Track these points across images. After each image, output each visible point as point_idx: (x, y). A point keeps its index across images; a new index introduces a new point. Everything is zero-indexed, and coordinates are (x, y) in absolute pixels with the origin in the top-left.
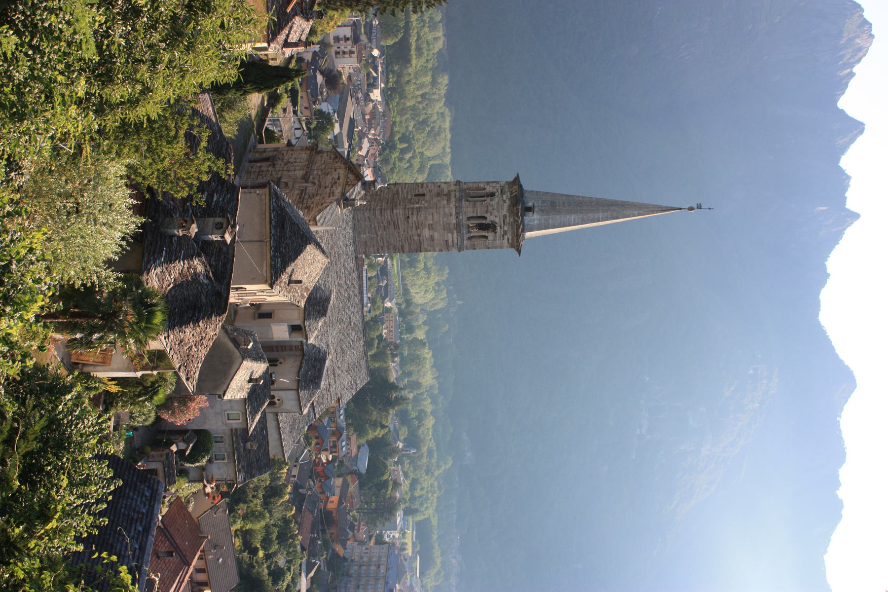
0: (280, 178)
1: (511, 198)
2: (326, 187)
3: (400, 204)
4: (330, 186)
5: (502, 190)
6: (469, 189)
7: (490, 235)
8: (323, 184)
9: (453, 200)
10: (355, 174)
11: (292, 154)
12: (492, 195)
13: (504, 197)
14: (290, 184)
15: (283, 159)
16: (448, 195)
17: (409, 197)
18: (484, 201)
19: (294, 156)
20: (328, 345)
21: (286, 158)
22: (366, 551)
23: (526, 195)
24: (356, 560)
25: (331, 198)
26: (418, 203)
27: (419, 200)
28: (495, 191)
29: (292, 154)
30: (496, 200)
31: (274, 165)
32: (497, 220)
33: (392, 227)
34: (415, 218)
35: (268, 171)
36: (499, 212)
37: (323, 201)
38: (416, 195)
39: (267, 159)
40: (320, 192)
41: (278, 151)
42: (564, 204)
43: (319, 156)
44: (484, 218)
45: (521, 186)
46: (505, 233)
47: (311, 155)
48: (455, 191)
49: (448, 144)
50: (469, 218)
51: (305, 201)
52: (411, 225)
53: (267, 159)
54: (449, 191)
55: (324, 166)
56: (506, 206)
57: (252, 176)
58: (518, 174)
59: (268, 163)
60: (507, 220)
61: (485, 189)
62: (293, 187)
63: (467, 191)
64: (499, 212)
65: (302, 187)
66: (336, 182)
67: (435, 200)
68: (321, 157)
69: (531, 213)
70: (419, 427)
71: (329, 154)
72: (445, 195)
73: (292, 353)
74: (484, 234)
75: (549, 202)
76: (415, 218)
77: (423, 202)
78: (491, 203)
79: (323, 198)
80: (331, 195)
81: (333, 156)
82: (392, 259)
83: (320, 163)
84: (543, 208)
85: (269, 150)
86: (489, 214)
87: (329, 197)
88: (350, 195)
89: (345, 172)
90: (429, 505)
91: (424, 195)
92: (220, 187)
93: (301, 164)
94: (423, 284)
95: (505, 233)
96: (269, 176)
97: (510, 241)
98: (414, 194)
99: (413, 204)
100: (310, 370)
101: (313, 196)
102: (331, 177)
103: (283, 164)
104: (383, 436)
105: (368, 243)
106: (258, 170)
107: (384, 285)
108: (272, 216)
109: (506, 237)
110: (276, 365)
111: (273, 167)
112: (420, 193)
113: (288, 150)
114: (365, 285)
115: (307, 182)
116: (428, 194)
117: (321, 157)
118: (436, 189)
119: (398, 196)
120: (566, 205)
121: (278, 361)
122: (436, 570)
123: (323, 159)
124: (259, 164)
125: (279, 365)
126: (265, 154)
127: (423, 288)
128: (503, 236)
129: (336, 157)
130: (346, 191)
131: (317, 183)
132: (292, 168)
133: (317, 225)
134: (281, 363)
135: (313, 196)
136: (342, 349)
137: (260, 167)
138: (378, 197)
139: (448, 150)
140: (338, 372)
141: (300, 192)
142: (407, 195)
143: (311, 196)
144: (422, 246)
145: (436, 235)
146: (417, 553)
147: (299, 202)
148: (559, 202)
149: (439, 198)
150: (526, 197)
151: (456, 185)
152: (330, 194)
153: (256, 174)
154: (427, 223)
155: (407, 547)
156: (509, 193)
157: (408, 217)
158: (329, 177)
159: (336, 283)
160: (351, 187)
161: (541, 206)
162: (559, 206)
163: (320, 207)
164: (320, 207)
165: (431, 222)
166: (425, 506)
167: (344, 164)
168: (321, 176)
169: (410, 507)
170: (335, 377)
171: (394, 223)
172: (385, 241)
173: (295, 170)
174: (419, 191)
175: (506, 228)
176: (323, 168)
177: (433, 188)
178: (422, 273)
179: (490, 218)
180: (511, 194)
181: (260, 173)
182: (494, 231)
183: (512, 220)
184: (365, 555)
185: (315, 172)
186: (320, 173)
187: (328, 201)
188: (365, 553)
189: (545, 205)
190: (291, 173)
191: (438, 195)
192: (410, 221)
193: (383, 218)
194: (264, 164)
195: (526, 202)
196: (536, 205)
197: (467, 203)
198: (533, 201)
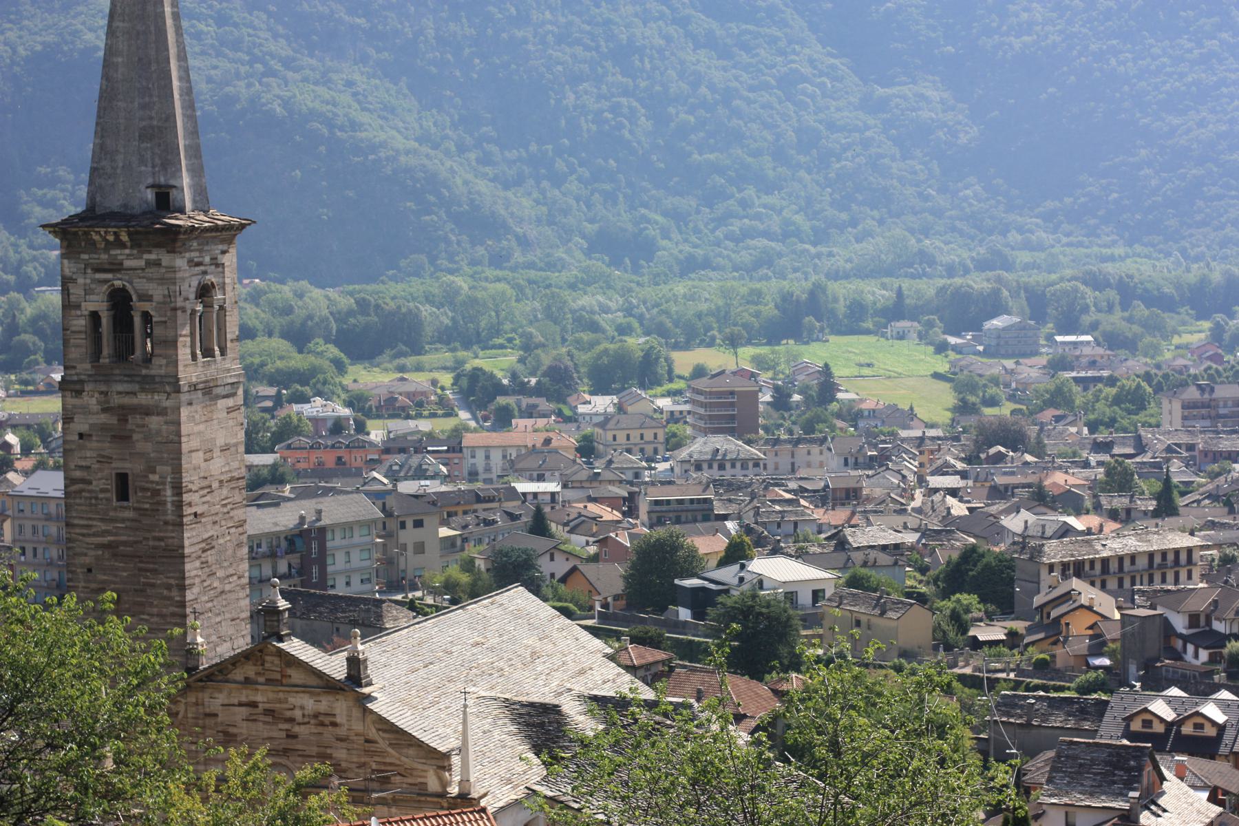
2: (291, 736)
3: (160, 539)
4: (286, 726)
6: (96, 354)
9: (143, 399)
12: (120, 301)
17: (129, 514)
18: (147, 317)
22: (29, 552)
24: (56, 575)
25: (338, 720)
26: (156, 493)
27: (144, 489)
40: (314, 750)
54: (105, 410)
56: (166, 259)
58: (44, 226)
61: (95, 317)
63: (104, 361)
66: (269, 712)
67: (141, 446)
69: (174, 193)
75: (144, 145)
80: (327, 720)
84: (158, 161)
87: (334, 724)
89: (220, 691)
98: (115, 503)
102: (245, 724)
118: (94, 445)
119: (125, 543)
120: (147, 99)
128: (217, 265)
129: (970, 708)
142: (123, 520)
148: (141, 119)
149: (135, 437)
150: (125, 206)
151: (79, 393)
152: (322, 724)
156: (113, 252)
157: (195, 515)
161: (153, 167)
162: (151, 118)
163: (382, 744)
164: (382, 744)
165: (201, 454)
171: (204, 551)
175: (207, 259)
180: (122, 245)
184: (39, 555)
188: (35, 555)
189: (148, 155)
191: (122, 437)
192: (199, 510)
196: (150, 181)
198: (142, 187)
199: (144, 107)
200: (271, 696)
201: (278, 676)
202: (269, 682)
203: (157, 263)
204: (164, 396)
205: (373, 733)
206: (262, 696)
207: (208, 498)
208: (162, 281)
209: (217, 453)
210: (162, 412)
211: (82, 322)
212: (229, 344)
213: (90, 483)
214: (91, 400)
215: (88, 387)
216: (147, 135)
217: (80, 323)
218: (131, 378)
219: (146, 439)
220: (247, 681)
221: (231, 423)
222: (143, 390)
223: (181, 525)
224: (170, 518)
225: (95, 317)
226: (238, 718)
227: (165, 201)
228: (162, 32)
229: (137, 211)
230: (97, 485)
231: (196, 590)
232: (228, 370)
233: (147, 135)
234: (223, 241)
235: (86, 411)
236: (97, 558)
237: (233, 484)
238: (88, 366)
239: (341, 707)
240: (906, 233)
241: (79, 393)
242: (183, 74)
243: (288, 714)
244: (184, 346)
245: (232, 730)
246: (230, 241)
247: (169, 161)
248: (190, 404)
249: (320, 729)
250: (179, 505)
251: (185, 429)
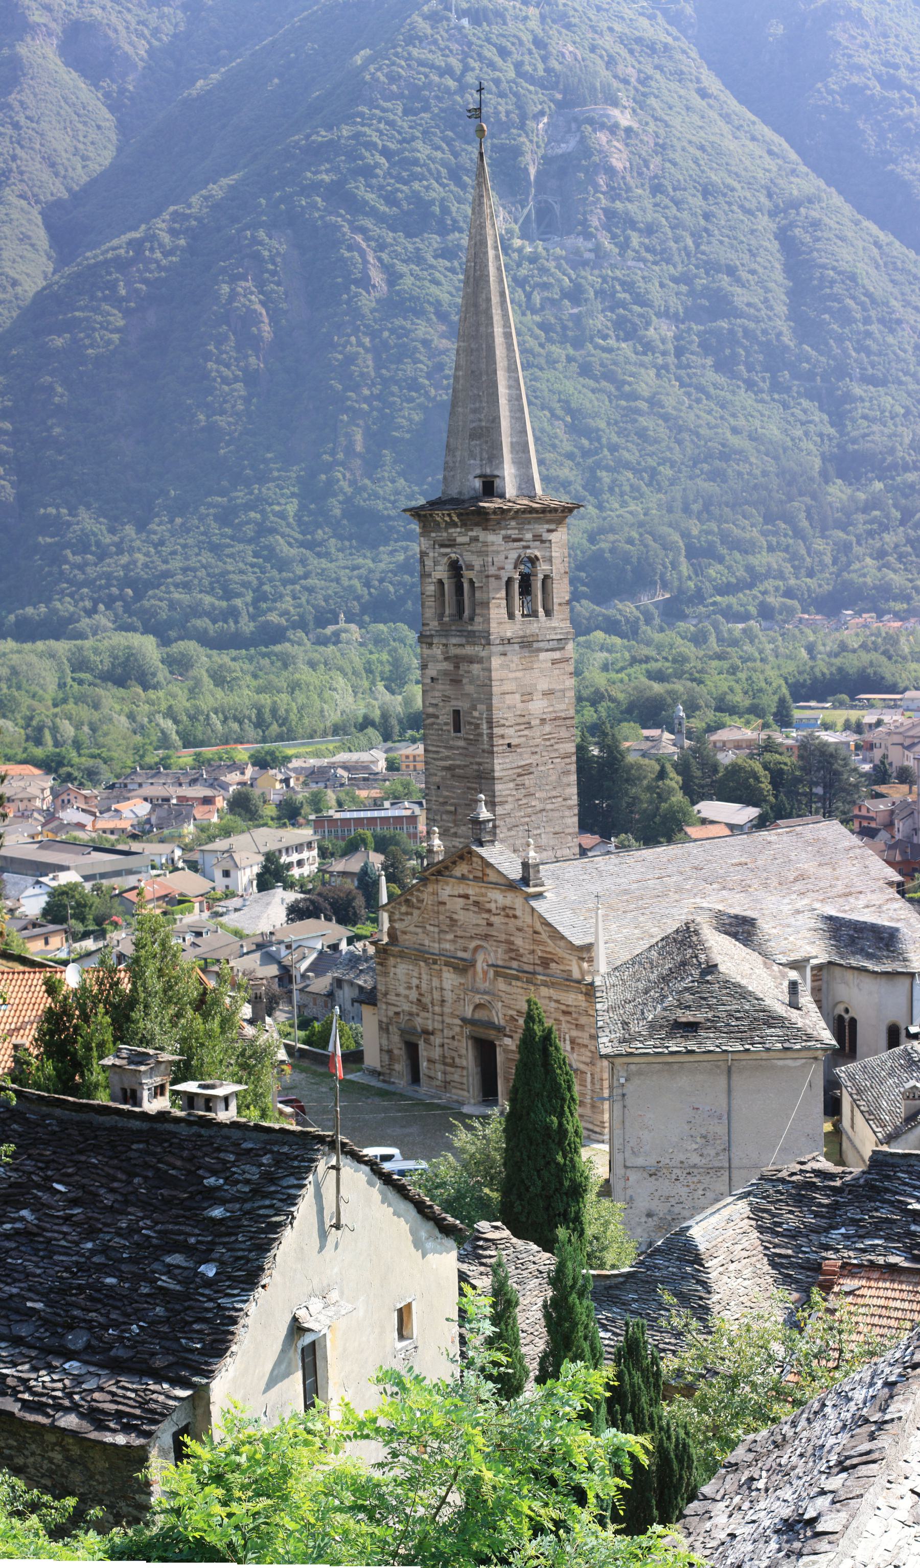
0: (464, 1020)
1: (464, 525)
2: (490, 925)
3: (480, 764)
4: (486, 916)
6: (441, 616)
7: (543, 568)
9: (469, 650)
10: (454, 863)
11: (398, 995)
12: (455, 568)
13: (460, 540)
14: (478, 999)
17: (461, 743)
18: (471, 582)
19: (402, 991)
20: (798, 912)
21: (406, 1007)
23: (453, 492)
25: (518, 913)
26: (477, 726)
27: (470, 723)
28: (445, 560)
29: (398, 995)
30: (466, 556)
31: (426, 1032)
33: (527, 780)
34: (511, 731)
35: (442, 1046)
36: (498, 552)
37: (530, 931)
38: (457, 729)
39: (412, 1050)
40: (503, 937)
42: (474, 411)
43: (402, 938)
44: (509, 581)
45: (434, 504)
46: (538, 538)
47: (402, 955)
48: (445, 645)
49: (28, 646)
50: (511, 616)
51: (529, 968)
53: (412, 1050)
54: (447, 659)
55: (432, 929)
56: (483, 535)
60: (514, 533)
61: (440, 582)
62: (485, 993)
63: (446, 619)
64: (498, 552)
65: (485, 973)
66: (476, 903)
67: (469, 689)
68: (404, 933)
69: (497, 482)
70: (612, 699)
71: (396, 917)
72: (457, 667)
73: (824, 987)
78: (477, 568)
79: (519, 930)
80: (511, 913)
81: (404, 909)
82: (288, 759)
83: (421, 936)
84: (485, 455)
85: (385, 1042)
86: (502, 573)
87: (515, 917)
88: (515, 873)
91: (457, 713)
93: (424, 976)
94: (320, 695)
95: (538, 538)
97: (553, 527)
99: (481, 735)
101: (513, 952)
104: (678, 774)
105: (557, 829)
106: (439, 1066)
107: (345, 774)
108: (675, 1049)
109: (546, 536)
110: (853, 1021)
111: (432, 1033)
112: (451, 721)
113: (387, 1004)
114: (355, 815)
115: (472, 964)
116: (454, 703)
117: (404, 933)
118: (440, 687)
119: (459, 767)
121: (840, 1017)
122: (884, 659)
123: (412, 929)
124: (424, 1064)
126: (396, 1052)
128: (543, 542)
131: (479, 942)
132: (436, 995)
133: (591, 945)
134: (847, 1011)
135: (512, 950)
136: (796, 880)
137: (430, 1061)
141: (500, 979)
142: (458, 748)
143: (513, 955)
144: (563, 715)
145: (543, 685)
147: (529, 982)
149: (465, 681)
150: (460, 493)
152: (507, 916)
153: (449, 1069)
154: (520, 705)
155: (853, 720)
157: (509, 745)
158: (461, 916)
159: (677, 897)
160: (488, 871)
163: (544, 936)
164: (544, 936)
166: (763, 685)
167: (425, 885)
168: (459, 933)
169: (775, 715)
170: (850, 894)
171: (519, 775)
172: (554, 793)
173: (442, 989)
174: (446, 724)
175: (529, 536)
177: (437, 694)
178: (301, 698)
180: (455, 525)
181: (448, 1063)
182: (533, 561)
185: (447, 946)
186: (450, 937)
190: (449, 996)
191: (456, 681)
192: (514, 742)
194: (423, 1052)
195: (472, 493)
196: (478, 472)
197: (478, 619)
198: (471, 477)
201: (480, 874)
202: (476, 878)
207: (526, 732)
208: (480, 553)
209: (537, 696)
210: (480, 661)
214: (437, 651)
215: (435, 641)
217: (431, 589)
218: (461, 633)
219: (471, 682)
220: (463, 878)
221: (556, 672)
223: (492, 753)
224: (486, 747)
225: (440, 582)
227: (490, 488)
228: (491, 349)
229: (466, 497)
231: (508, 807)
234: (549, 522)
236: (443, 778)
237: (558, 723)
239: (516, 901)
241: (430, 645)
243: (488, 906)
244: (499, 606)
245: (455, 917)
247: (495, 455)
249: (507, 920)
250: (491, 736)
251: (494, 675)
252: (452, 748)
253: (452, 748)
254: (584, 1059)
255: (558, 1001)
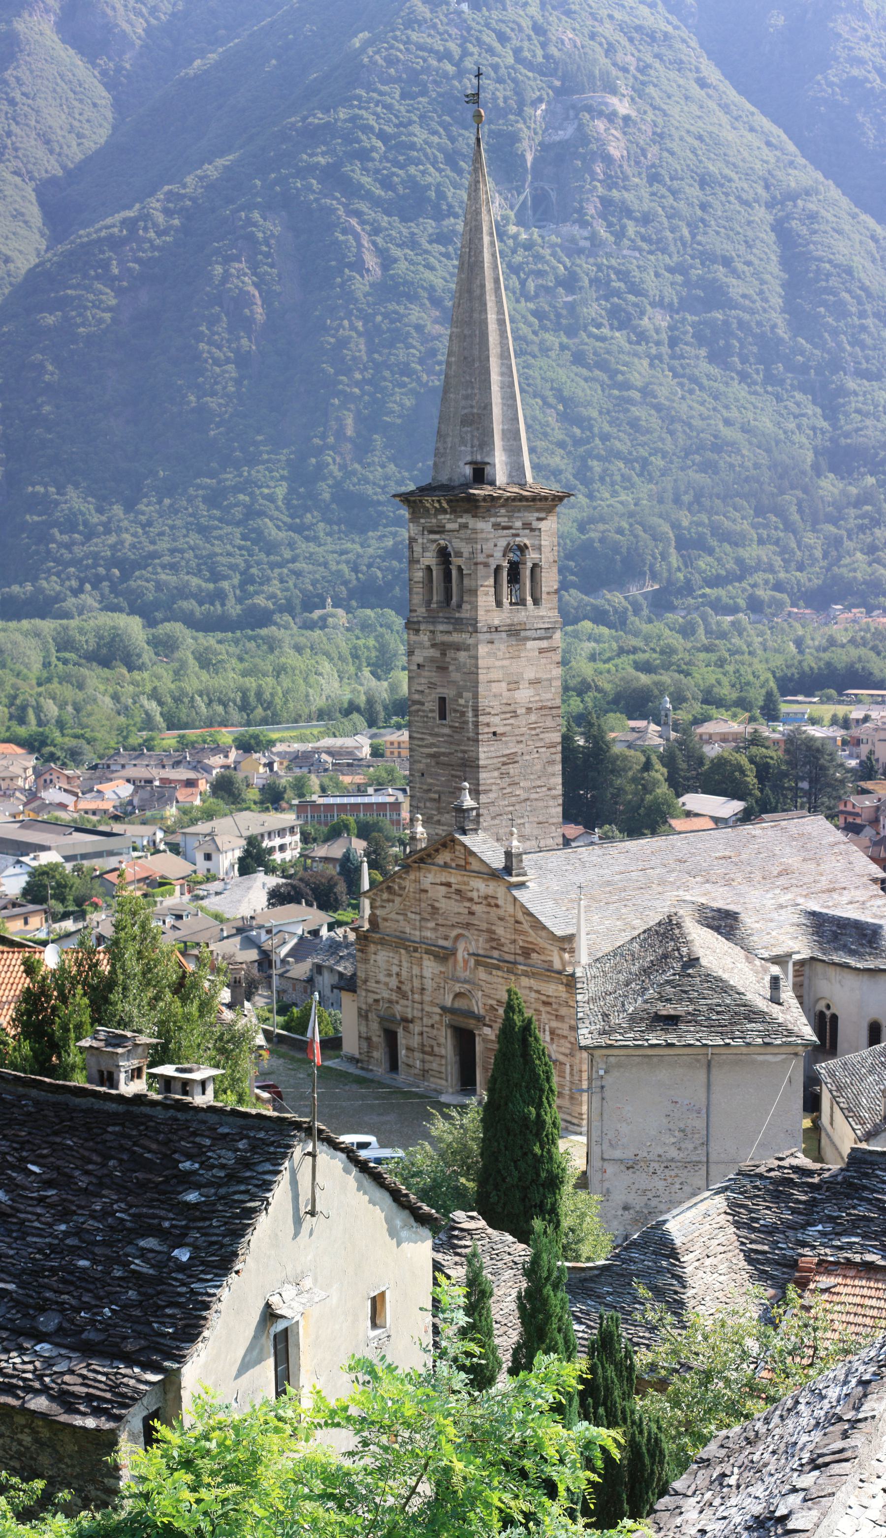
0: (443, 1008)
1: (454, 511)
2: (471, 913)
3: (465, 752)
4: (468, 904)
5: (431, 532)
6: (429, 602)
8: (465, 919)
9: (456, 637)
10: (437, 851)
11: (377, 982)
12: (444, 555)
14: (458, 988)
15: (390, 1002)
16: (444, 648)
17: (446, 731)
18: (460, 569)
19: (382, 978)
20: (781, 907)
23: (444, 478)
25: (500, 902)
26: (463, 714)
27: (456, 711)
28: (434, 546)
31: (406, 1020)
32: (502, 543)
33: (512, 769)
34: (496, 720)
35: (421, 1034)
36: (487, 540)
38: (443, 716)
39: (391, 1038)
40: (484, 926)
41: (367, 1011)
43: (382, 925)
45: (424, 490)
46: (527, 526)
47: (382, 942)
48: (432, 632)
49: (13, 624)
50: (499, 604)
52: (509, 728)
53: (391, 1038)
54: (433, 646)
56: (472, 522)
57: (435, 1066)
58: (394, 496)
59: (401, 1033)
60: (503, 521)
61: (429, 569)
62: (466, 981)
63: (434, 606)
64: (487, 540)
65: (466, 962)
66: (458, 892)
67: (455, 676)
68: (385, 920)
69: (488, 469)
70: (599, 690)
71: (378, 904)
72: (444, 654)
74: (528, 572)
76: (496, 720)
77: (462, 701)
78: (466, 555)
80: (493, 902)
81: (385, 896)
83: (402, 923)
84: (476, 442)
85: (364, 1029)
86: (491, 560)
87: (497, 906)
89: (430, 871)
90: (749, 670)
91: (442, 700)
92: (865, 1194)
94: (305, 680)
95: (527, 526)
96: (435, 1032)
97: (542, 515)
99: (466, 722)
100: (845, 946)
102: (444, 900)
103: (403, 1002)
104: (664, 765)
106: (417, 1055)
107: (329, 759)
109: (535, 524)
110: (834, 1018)
111: (412, 1021)
112: (436, 708)
114: (339, 800)
115: (453, 952)
116: (440, 690)
117: (385, 920)
118: (426, 674)
119: (444, 754)
123: (393, 916)
125: (833, 1010)
126: (375, 1039)
127: (313, 678)
128: (532, 530)
130: (484, 869)
131: (460, 931)
132: (416, 983)
134: (828, 1007)
135: (493, 940)
136: (780, 875)
137: (409, 1049)
138: (443, 798)
139: (25, 624)
140: (824, 883)
141: (481, 968)
142: (443, 735)
143: (494, 944)
145: (530, 674)
146: (840, 694)
148: (464, 408)
149: (451, 668)
150: (450, 479)
151: (417, 631)
152: (489, 905)
153: (427, 1057)
154: (506, 694)
155: (841, 715)
156: (440, 517)
157: (494, 734)
163: (526, 926)
164: (526, 926)
165: (504, 685)
167: (407, 872)
168: (440, 922)
171: (504, 764)
172: (539, 783)
173: (422, 977)
174: (432, 711)
175: (518, 524)
176: (418, 917)
177: (423, 681)
178: (286, 682)
179: (499, 559)
180: (445, 512)
181: (427, 1051)
183: (503, 511)
185: (428, 934)
187: (510, 909)
190: (429, 984)
191: (443, 669)
192: (499, 730)
193: (494, 787)
194: (402, 1041)
195: (462, 480)
197: (466, 606)
198: (461, 464)
199: (467, 397)
200: (460, 878)
201: (462, 863)
202: (458, 866)
203: (465, 526)
204: (468, 635)
205: (520, 916)
206: (454, 878)
207: (511, 721)
209: (524, 685)
210: (467, 648)
211: (420, 574)
212: (544, 596)
213: (423, 704)
215: (422, 627)
216: (467, 421)
217: (419, 575)
219: (458, 670)
220: (446, 866)
221: (543, 661)
222: (455, 630)
223: (477, 741)
224: (471, 735)
225: (429, 569)
226: (440, 895)
227: (480, 475)
229: (457, 483)
230: (428, 706)
231: (492, 795)
232: (542, 617)
233: (467, 421)
234: (539, 510)
235: (421, 644)
236: (427, 765)
237: (543, 712)
238: (423, 610)
240: (291, 533)
242: (505, 370)
243: (470, 894)
244: (487, 594)
245: (437, 905)
246: (550, 510)
247: (485, 442)
248: (491, 642)
249: (488, 909)
250: (476, 724)
252: (437, 735)
253: (437, 735)
254: (563, 1050)
255: (538, 992)
